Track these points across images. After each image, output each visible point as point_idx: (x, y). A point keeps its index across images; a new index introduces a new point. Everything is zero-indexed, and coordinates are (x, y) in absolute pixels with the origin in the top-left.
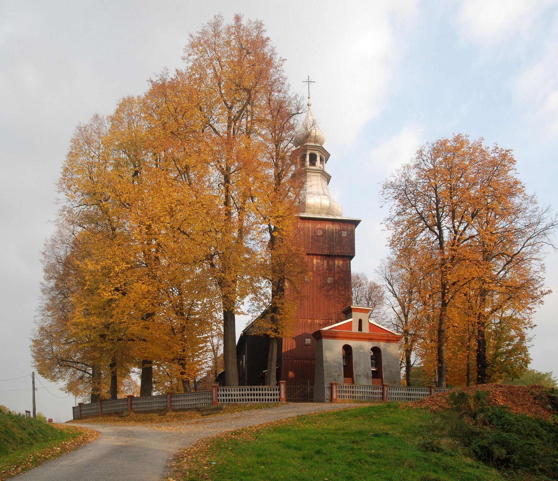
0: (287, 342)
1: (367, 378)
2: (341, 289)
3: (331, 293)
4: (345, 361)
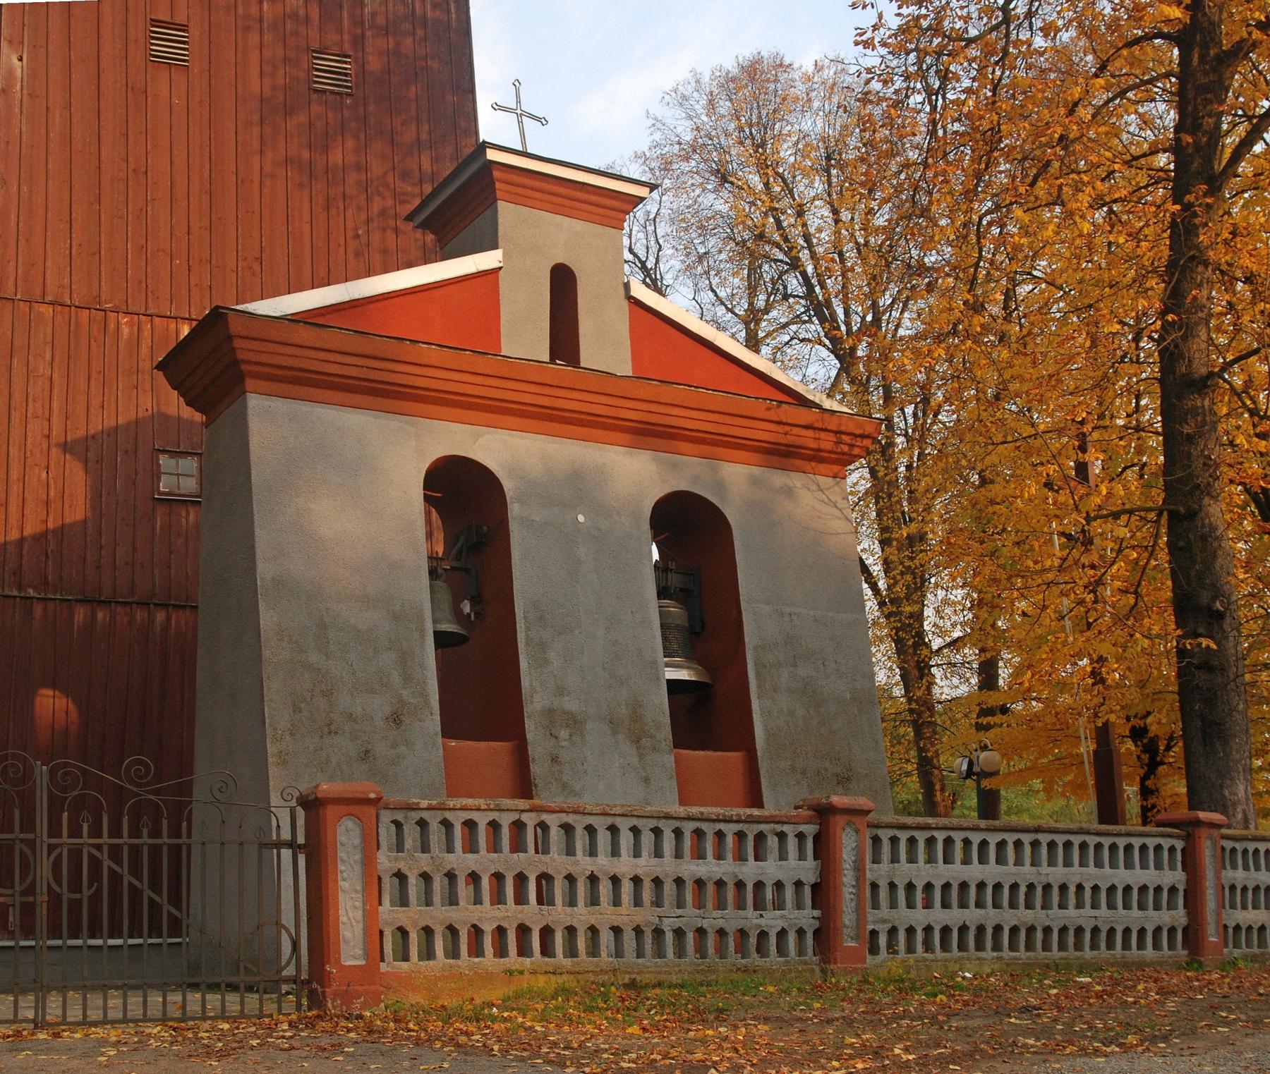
0: (15, 475)
1: (637, 741)
2: (409, 136)
3: (336, 157)
4: (445, 596)
